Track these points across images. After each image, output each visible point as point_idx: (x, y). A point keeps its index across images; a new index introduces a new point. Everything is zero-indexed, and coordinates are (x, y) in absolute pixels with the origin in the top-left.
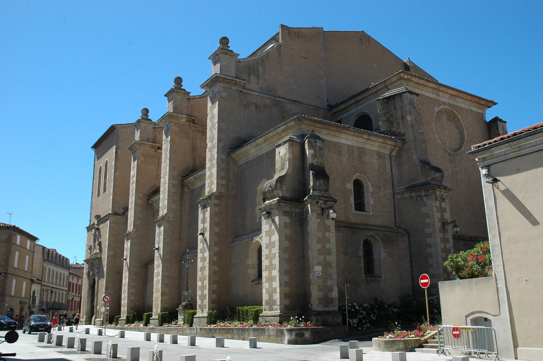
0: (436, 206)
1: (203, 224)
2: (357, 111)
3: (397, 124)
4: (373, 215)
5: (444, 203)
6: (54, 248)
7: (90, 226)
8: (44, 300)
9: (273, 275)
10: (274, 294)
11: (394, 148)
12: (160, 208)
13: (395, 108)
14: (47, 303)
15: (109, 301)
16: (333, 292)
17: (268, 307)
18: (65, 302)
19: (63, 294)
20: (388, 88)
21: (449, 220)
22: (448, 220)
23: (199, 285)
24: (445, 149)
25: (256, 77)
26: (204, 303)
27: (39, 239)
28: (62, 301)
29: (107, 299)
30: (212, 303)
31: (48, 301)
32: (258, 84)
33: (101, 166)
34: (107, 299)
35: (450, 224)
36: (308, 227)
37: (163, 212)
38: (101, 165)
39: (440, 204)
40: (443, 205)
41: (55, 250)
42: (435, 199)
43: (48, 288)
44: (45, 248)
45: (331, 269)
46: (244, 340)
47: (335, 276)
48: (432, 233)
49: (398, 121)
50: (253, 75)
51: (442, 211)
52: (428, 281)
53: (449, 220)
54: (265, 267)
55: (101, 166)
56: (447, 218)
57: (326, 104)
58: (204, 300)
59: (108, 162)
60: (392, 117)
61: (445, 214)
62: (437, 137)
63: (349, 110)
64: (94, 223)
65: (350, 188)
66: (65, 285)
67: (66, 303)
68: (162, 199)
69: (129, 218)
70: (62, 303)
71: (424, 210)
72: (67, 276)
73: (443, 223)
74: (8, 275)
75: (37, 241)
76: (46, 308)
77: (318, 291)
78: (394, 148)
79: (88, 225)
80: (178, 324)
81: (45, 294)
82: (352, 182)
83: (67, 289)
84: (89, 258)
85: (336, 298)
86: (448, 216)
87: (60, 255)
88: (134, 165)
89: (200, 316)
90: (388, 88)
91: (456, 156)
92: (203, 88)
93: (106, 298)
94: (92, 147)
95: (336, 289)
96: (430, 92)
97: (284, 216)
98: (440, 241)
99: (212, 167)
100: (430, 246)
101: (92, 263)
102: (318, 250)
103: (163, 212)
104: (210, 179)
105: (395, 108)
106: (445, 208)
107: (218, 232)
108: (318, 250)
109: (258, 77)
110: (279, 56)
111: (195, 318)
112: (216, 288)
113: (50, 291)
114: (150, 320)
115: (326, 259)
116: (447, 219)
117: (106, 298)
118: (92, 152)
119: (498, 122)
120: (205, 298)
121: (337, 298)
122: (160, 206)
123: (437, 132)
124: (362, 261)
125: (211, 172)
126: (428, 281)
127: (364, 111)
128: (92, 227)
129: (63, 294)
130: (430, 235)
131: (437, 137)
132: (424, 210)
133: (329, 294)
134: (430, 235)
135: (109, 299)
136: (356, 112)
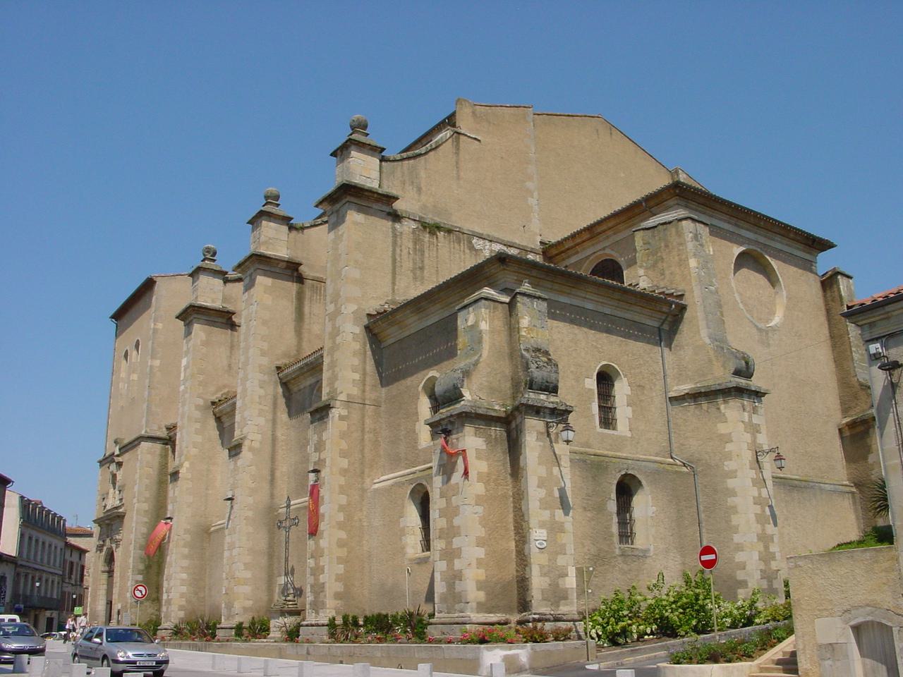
0: (743, 422)
1: (318, 454)
2: (594, 253)
3: (671, 274)
4: (631, 438)
5: (755, 415)
6: (40, 500)
7: (106, 458)
8: (21, 592)
9: (454, 546)
10: (457, 582)
11: (667, 317)
12: (236, 424)
13: (667, 246)
14: (26, 597)
15: (144, 596)
16: (567, 578)
17: (445, 606)
18: (57, 596)
19: (53, 582)
20: (651, 212)
21: (766, 448)
22: (764, 446)
23: (311, 566)
24: (752, 322)
25: (415, 189)
26: (321, 600)
27: (13, 482)
28: (46, 593)
29: (141, 591)
30: (335, 599)
31: (28, 593)
32: (419, 201)
33: (127, 351)
34: (141, 591)
35: (768, 453)
36: (521, 457)
37: (241, 431)
38: (128, 348)
39: (750, 417)
40: (755, 419)
41: (41, 502)
42: (742, 409)
43: (28, 571)
44: (24, 497)
45: (563, 534)
46: (401, 668)
47: (570, 549)
48: (736, 471)
49: (673, 268)
50: (410, 185)
51: (754, 429)
52: (714, 558)
53: (766, 448)
54: (440, 532)
55: (127, 351)
56: (761, 442)
57: (539, 239)
58: (321, 594)
59: (140, 343)
60: (662, 262)
61: (758, 435)
62: (738, 299)
63: (579, 250)
64: (113, 454)
65: (592, 388)
66: (57, 564)
67: (59, 597)
68: (240, 408)
69: (177, 443)
70: (51, 599)
71: (722, 428)
72: (61, 549)
73: (756, 452)
74: (462, 137)
75: (9, 485)
76: (24, 607)
77: (541, 576)
78: (667, 317)
79: (101, 457)
80: (271, 638)
81: (22, 580)
82: (595, 377)
83: (61, 573)
84: (102, 515)
85: (572, 588)
86: (763, 440)
87: (49, 511)
88: (188, 348)
89: (313, 622)
90: (651, 212)
91: (770, 334)
92: (320, 207)
93: (138, 590)
94: (113, 317)
95: (572, 572)
96: (725, 221)
97: (476, 436)
98: (751, 485)
99: (335, 349)
100: (733, 493)
101: (108, 525)
102: (541, 500)
103: (241, 431)
104: (330, 371)
105: (667, 246)
106: (759, 425)
107: (346, 467)
108: (541, 500)
109: (419, 190)
110: (456, 153)
111: (302, 626)
112: (342, 571)
113: (30, 577)
114: (217, 631)
115: (554, 516)
116: (762, 444)
117: (138, 590)
118: (112, 325)
119: (839, 277)
120: (321, 590)
121: (575, 590)
122: (236, 420)
123: (737, 290)
124: (614, 521)
125: (332, 357)
126: (714, 558)
127: (608, 251)
128: (109, 459)
129: (53, 582)
130: (732, 474)
131: (738, 299)
132: (722, 428)
133: (560, 581)
134: (732, 474)
135: (144, 593)
136: (592, 254)
